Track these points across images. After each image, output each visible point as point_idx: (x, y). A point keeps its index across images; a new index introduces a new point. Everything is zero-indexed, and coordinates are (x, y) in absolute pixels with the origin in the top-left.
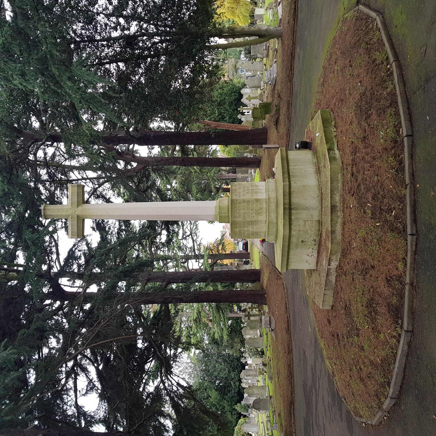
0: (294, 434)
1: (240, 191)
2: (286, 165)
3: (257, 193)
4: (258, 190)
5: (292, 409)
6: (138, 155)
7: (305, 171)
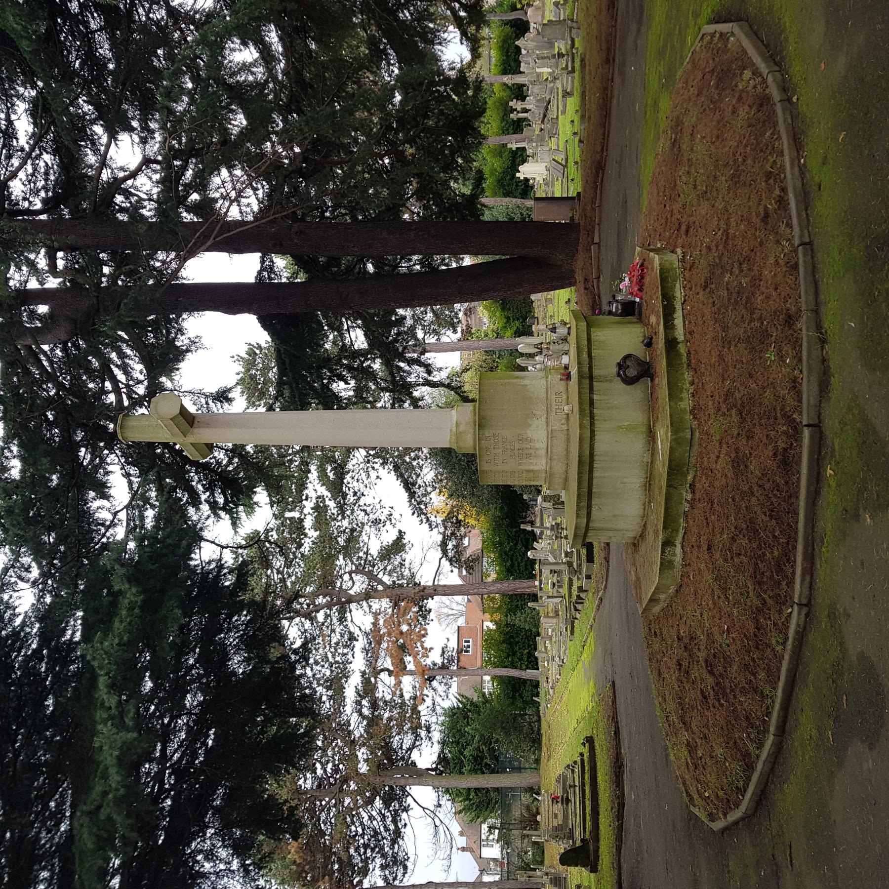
0: (597, 226)
1: (496, 451)
2: (586, 477)
3: (528, 456)
4: (531, 451)
5: (600, 179)
6: (230, 219)
7: (622, 483)
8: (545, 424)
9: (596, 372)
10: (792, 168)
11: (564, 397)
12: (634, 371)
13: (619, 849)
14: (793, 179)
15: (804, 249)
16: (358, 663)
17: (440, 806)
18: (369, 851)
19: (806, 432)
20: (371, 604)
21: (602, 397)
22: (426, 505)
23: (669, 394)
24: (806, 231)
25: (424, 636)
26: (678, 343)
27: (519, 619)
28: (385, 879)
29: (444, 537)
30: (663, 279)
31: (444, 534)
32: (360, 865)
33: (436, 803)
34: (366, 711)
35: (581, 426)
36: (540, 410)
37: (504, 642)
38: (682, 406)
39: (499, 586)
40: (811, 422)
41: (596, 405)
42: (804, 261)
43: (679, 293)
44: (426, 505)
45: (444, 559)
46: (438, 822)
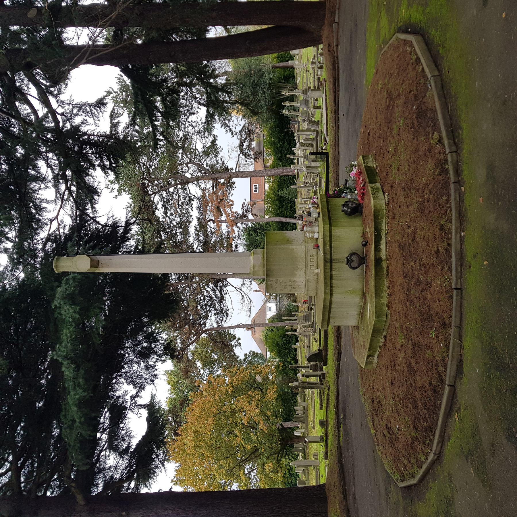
0: (337, 10)
1: (276, 286)
8: (304, 274)
9: (334, 257)
10: (456, 235)
11: (316, 258)
12: (357, 260)
13: (338, 375)
14: (455, 243)
15: (457, 292)
16: (195, 213)
17: (244, 284)
18: (208, 307)
19: (447, 389)
20: (200, 184)
21: (338, 272)
22: (229, 121)
23: (376, 294)
24: (459, 281)
25: (232, 205)
26: (382, 261)
27: (285, 193)
28: (217, 322)
29: (241, 142)
30: (376, 217)
31: (241, 139)
32: (204, 314)
33: (242, 283)
34: (201, 238)
35: (325, 293)
36: (301, 265)
37: (277, 200)
38: (382, 302)
39: (274, 172)
40: (450, 384)
41: (333, 278)
42: (457, 299)
43: (384, 227)
44: (229, 121)
45: (241, 155)
46: (243, 293)
